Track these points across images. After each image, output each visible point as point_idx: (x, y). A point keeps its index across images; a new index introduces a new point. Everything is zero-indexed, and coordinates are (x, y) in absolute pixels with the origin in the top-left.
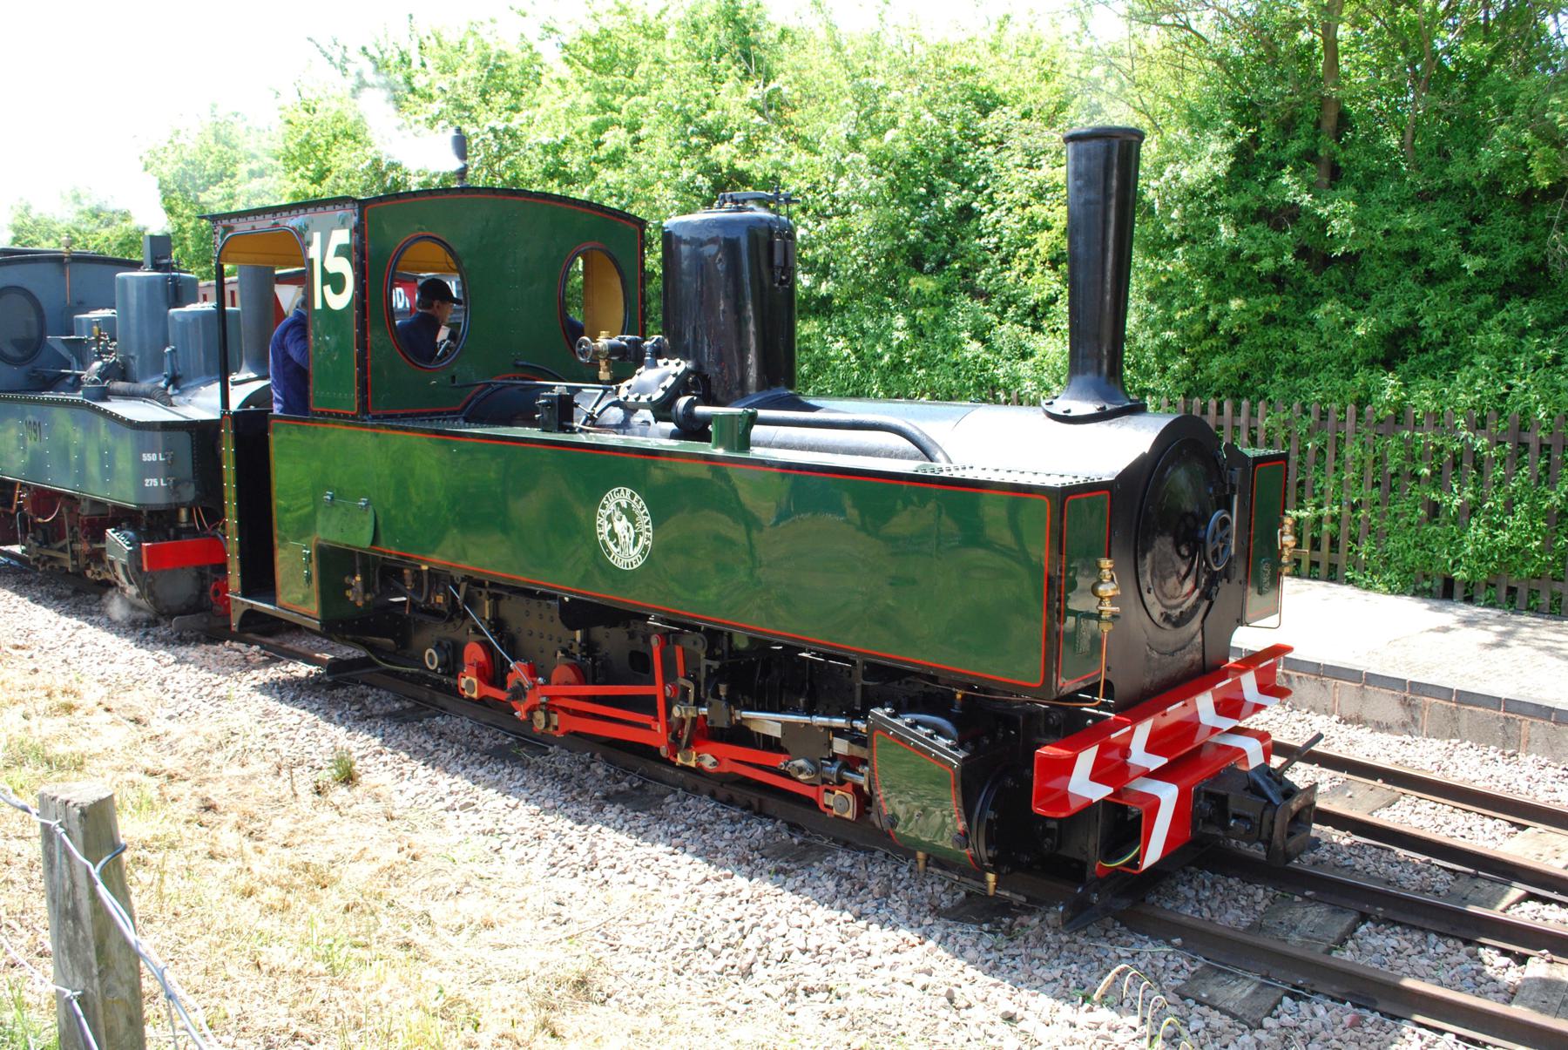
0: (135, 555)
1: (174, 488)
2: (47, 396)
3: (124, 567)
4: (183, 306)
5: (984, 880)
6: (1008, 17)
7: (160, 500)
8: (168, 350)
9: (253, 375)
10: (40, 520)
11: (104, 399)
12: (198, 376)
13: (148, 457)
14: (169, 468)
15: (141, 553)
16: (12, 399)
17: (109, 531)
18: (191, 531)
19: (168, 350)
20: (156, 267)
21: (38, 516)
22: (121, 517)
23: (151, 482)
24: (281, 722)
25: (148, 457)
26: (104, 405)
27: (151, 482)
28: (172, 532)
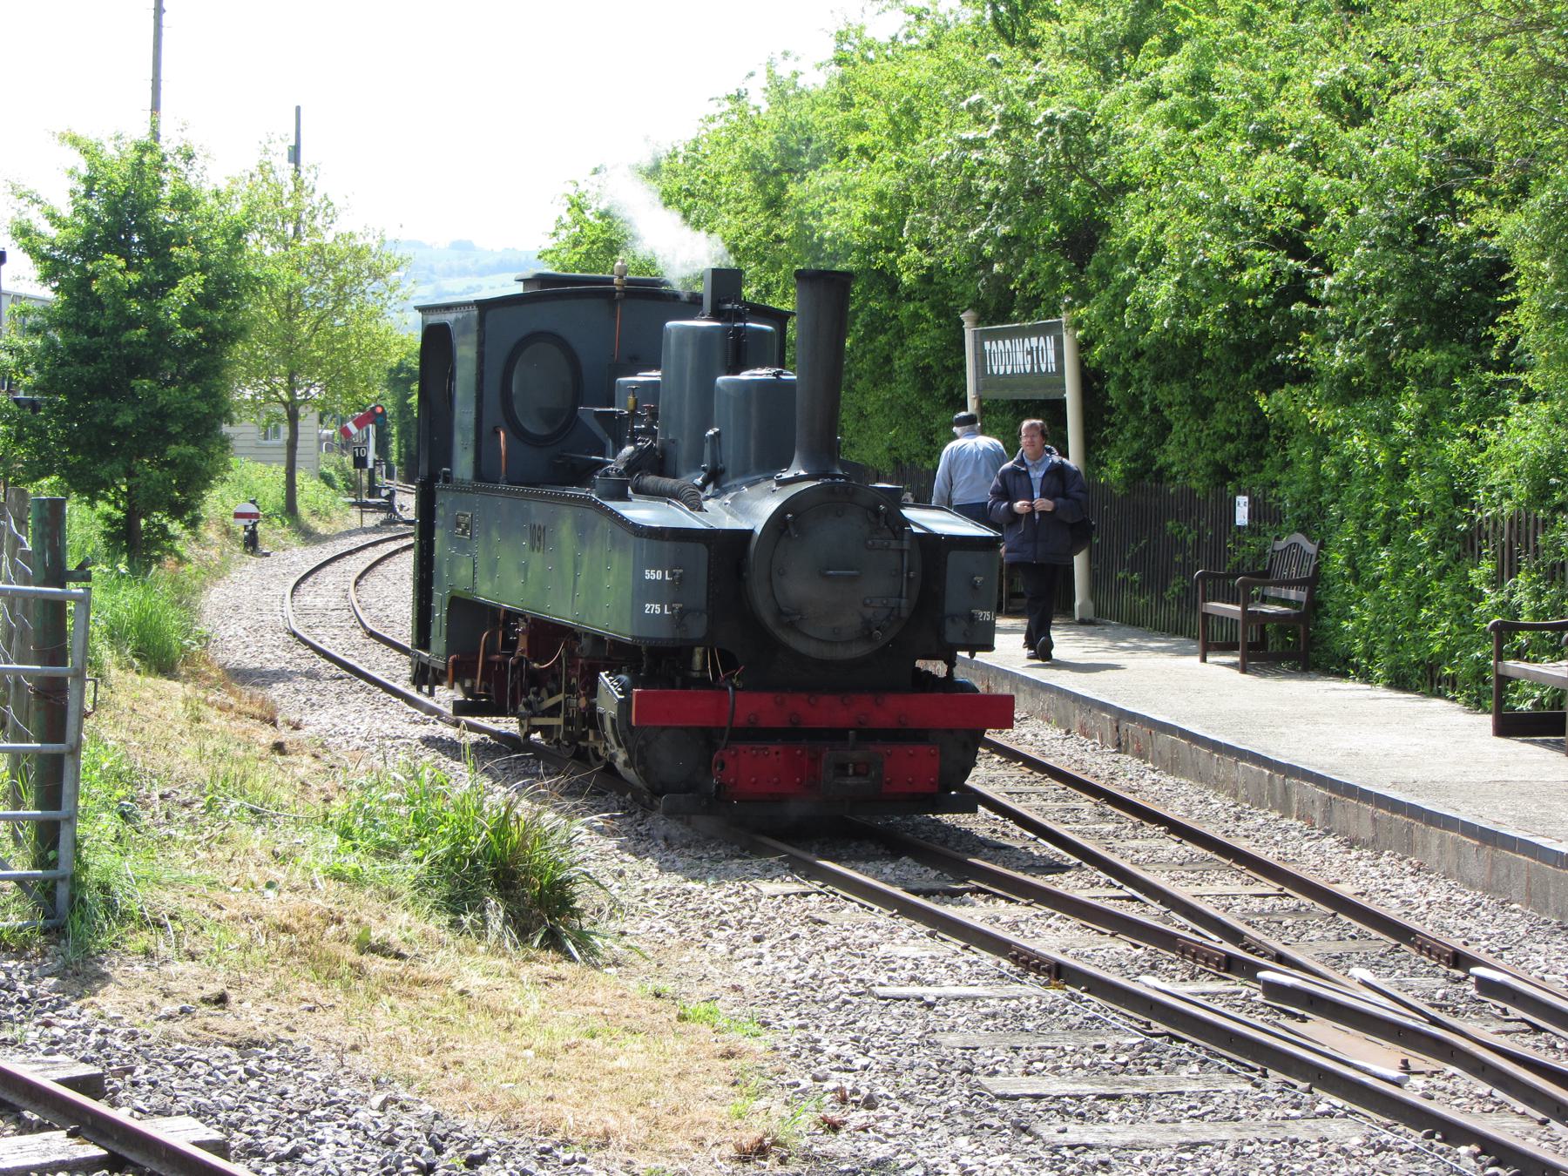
0: (624, 705)
1: (680, 617)
2: (573, 491)
3: (613, 721)
4: (737, 373)
5: (592, 688)
6: (72, 173)
7: (664, 633)
8: (711, 432)
9: (802, 473)
10: (536, 665)
11: (623, 497)
12: (744, 472)
13: (652, 575)
14: (674, 590)
15: (631, 700)
16: (517, 493)
17: (602, 674)
18: (703, 682)
19: (711, 432)
20: (716, 314)
21: (535, 661)
22: (616, 654)
23: (653, 608)
24: (974, 1079)
25: (652, 575)
26: (611, 504)
27: (653, 608)
28: (678, 680)
